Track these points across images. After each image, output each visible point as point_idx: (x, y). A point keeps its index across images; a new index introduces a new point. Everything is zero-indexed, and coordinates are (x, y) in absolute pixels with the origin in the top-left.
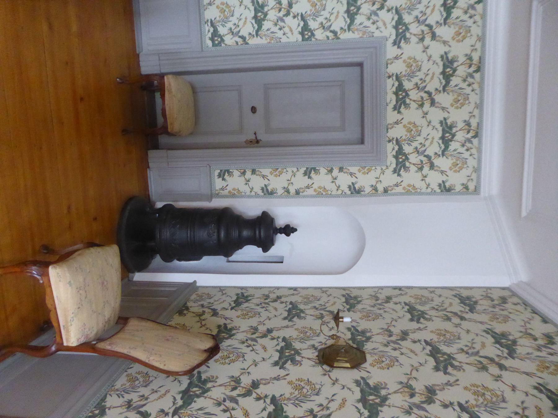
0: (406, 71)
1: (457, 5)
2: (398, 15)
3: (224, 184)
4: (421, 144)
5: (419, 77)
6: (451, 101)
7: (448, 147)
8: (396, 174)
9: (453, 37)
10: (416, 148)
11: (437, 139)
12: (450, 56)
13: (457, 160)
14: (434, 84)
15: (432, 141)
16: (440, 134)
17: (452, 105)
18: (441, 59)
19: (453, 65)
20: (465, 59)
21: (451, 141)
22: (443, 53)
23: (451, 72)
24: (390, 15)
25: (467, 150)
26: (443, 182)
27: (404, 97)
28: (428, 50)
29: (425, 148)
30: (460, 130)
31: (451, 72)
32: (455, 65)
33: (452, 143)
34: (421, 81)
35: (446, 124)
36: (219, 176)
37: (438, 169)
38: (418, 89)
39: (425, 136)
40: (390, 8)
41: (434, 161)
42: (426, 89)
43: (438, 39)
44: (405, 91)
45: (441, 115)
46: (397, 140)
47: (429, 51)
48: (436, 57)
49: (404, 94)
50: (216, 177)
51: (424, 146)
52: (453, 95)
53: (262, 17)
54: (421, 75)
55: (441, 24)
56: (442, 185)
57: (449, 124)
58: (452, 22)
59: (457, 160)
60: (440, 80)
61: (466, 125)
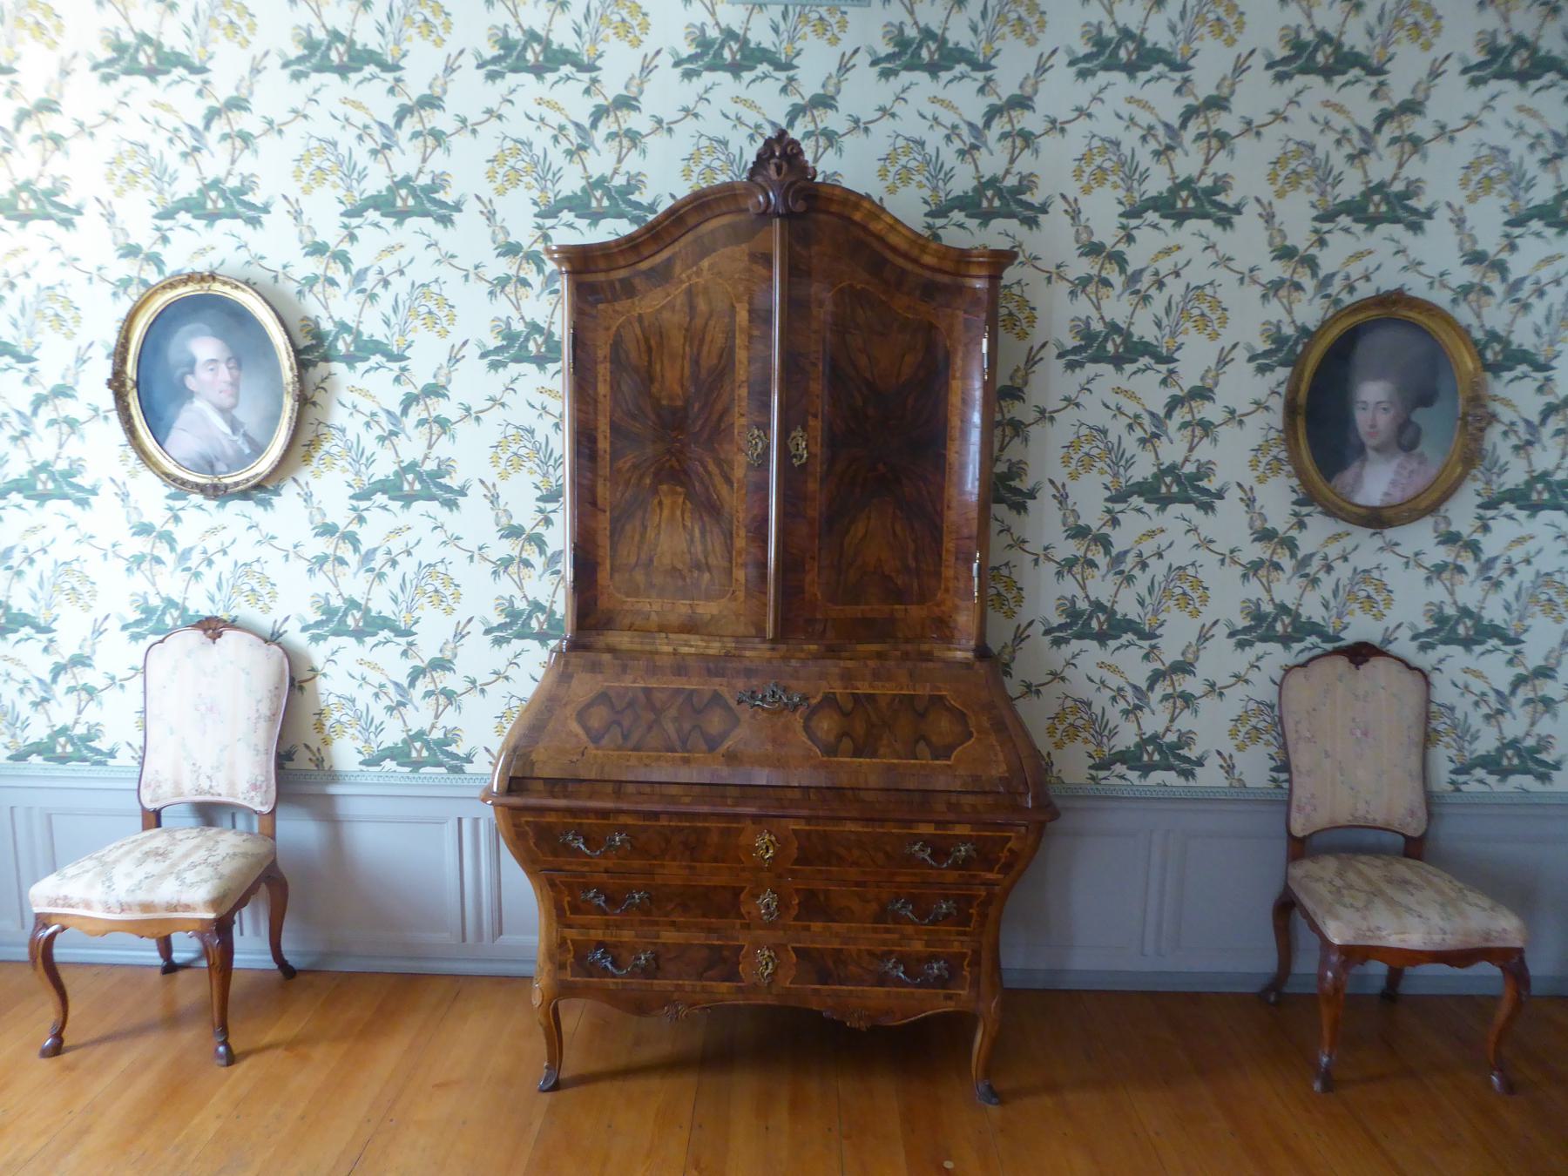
0: (335, 186)
2: (1338, 214)
3: (1213, 762)
4: (948, 138)
8: (456, 216)
9: (241, 46)
10: (570, 153)
13: (1205, 22)
14: (1162, 98)
17: (1196, 613)
18: (303, 80)
19: (1110, 41)
22: (96, 75)
23: (342, 48)
24: (1336, 240)
27: (999, 193)
28: (88, 123)
31: (342, 48)
34: (177, 141)
36: (1187, 774)
39: (1317, 128)
40: (1314, 237)
41: (1397, 101)
44: (982, 187)
46: (159, 216)
48: (885, 91)
49: (403, 192)
50: (1548, 788)
52: (1003, 37)
53: (358, 615)
54: (1130, 140)
55: (594, 81)
56: (1083, 65)
58: (391, 46)
59: (1205, 22)
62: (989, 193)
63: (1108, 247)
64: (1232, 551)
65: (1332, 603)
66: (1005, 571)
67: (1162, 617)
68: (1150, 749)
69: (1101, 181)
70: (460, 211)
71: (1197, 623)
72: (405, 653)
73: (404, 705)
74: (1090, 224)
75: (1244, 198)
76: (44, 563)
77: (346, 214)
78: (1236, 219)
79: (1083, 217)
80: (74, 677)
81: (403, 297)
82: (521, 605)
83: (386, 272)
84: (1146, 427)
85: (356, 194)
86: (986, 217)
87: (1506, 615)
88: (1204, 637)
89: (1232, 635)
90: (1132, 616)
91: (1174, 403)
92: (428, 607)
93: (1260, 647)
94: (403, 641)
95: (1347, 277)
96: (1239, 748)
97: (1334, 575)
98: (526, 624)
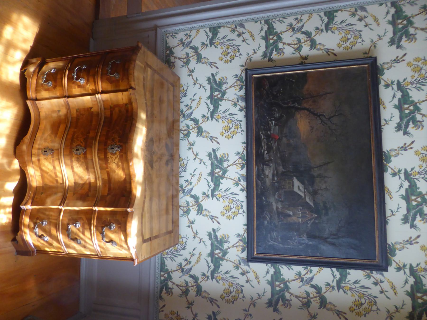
1: (225, 97)
5: (184, 257)
6: (221, 130)
7: (218, 108)
11: (204, 99)
12: (219, 234)
15: (199, 258)
16: (208, 93)
17: (222, 134)
19: (221, 88)
20: (237, 240)
21: (222, 178)
23: (220, 255)
25: (239, 36)
26: (213, 75)
29: (191, 110)
30: (231, 87)
32: (225, 164)
33: (223, 103)
35: (215, 80)
37: (207, 61)
38: (183, 46)
42: (192, 193)
43: (204, 134)
45: (209, 146)
47: (195, 75)
51: (190, 262)
57: (219, 156)
60: (208, 263)
61: (240, 158)
62: (412, 108)
63: (394, 258)
64: (251, 315)
65: (228, 275)
66: (238, 54)
67: (221, 199)
68: (166, 275)
69: (414, 70)
70: (397, 48)
71: (218, 135)
72: (204, 116)
73: (182, 271)
74: (393, 67)
75: (405, 49)
76: (238, 41)
77: (398, 82)
78: (408, 225)
79: (396, 64)
80: (193, 56)
81: (355, 27)
82: (226, 246)
83: (365, 19)
84: (306, 276)
85: (409, 87)
86: (400, 107)
87: (224, 271)
88: (212, 139)
89: (214, 150)
90: (221, 186)
91: (308, 34)
92: (224, 205)
93: (209, 243)
94: (210, 193)
95: (382, 282)
96: (166, 315)
97: (240, 276)
98: (217, 167)
